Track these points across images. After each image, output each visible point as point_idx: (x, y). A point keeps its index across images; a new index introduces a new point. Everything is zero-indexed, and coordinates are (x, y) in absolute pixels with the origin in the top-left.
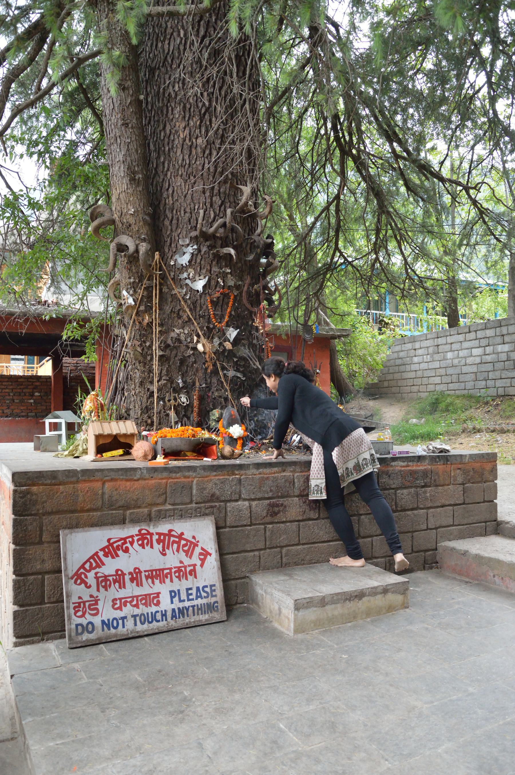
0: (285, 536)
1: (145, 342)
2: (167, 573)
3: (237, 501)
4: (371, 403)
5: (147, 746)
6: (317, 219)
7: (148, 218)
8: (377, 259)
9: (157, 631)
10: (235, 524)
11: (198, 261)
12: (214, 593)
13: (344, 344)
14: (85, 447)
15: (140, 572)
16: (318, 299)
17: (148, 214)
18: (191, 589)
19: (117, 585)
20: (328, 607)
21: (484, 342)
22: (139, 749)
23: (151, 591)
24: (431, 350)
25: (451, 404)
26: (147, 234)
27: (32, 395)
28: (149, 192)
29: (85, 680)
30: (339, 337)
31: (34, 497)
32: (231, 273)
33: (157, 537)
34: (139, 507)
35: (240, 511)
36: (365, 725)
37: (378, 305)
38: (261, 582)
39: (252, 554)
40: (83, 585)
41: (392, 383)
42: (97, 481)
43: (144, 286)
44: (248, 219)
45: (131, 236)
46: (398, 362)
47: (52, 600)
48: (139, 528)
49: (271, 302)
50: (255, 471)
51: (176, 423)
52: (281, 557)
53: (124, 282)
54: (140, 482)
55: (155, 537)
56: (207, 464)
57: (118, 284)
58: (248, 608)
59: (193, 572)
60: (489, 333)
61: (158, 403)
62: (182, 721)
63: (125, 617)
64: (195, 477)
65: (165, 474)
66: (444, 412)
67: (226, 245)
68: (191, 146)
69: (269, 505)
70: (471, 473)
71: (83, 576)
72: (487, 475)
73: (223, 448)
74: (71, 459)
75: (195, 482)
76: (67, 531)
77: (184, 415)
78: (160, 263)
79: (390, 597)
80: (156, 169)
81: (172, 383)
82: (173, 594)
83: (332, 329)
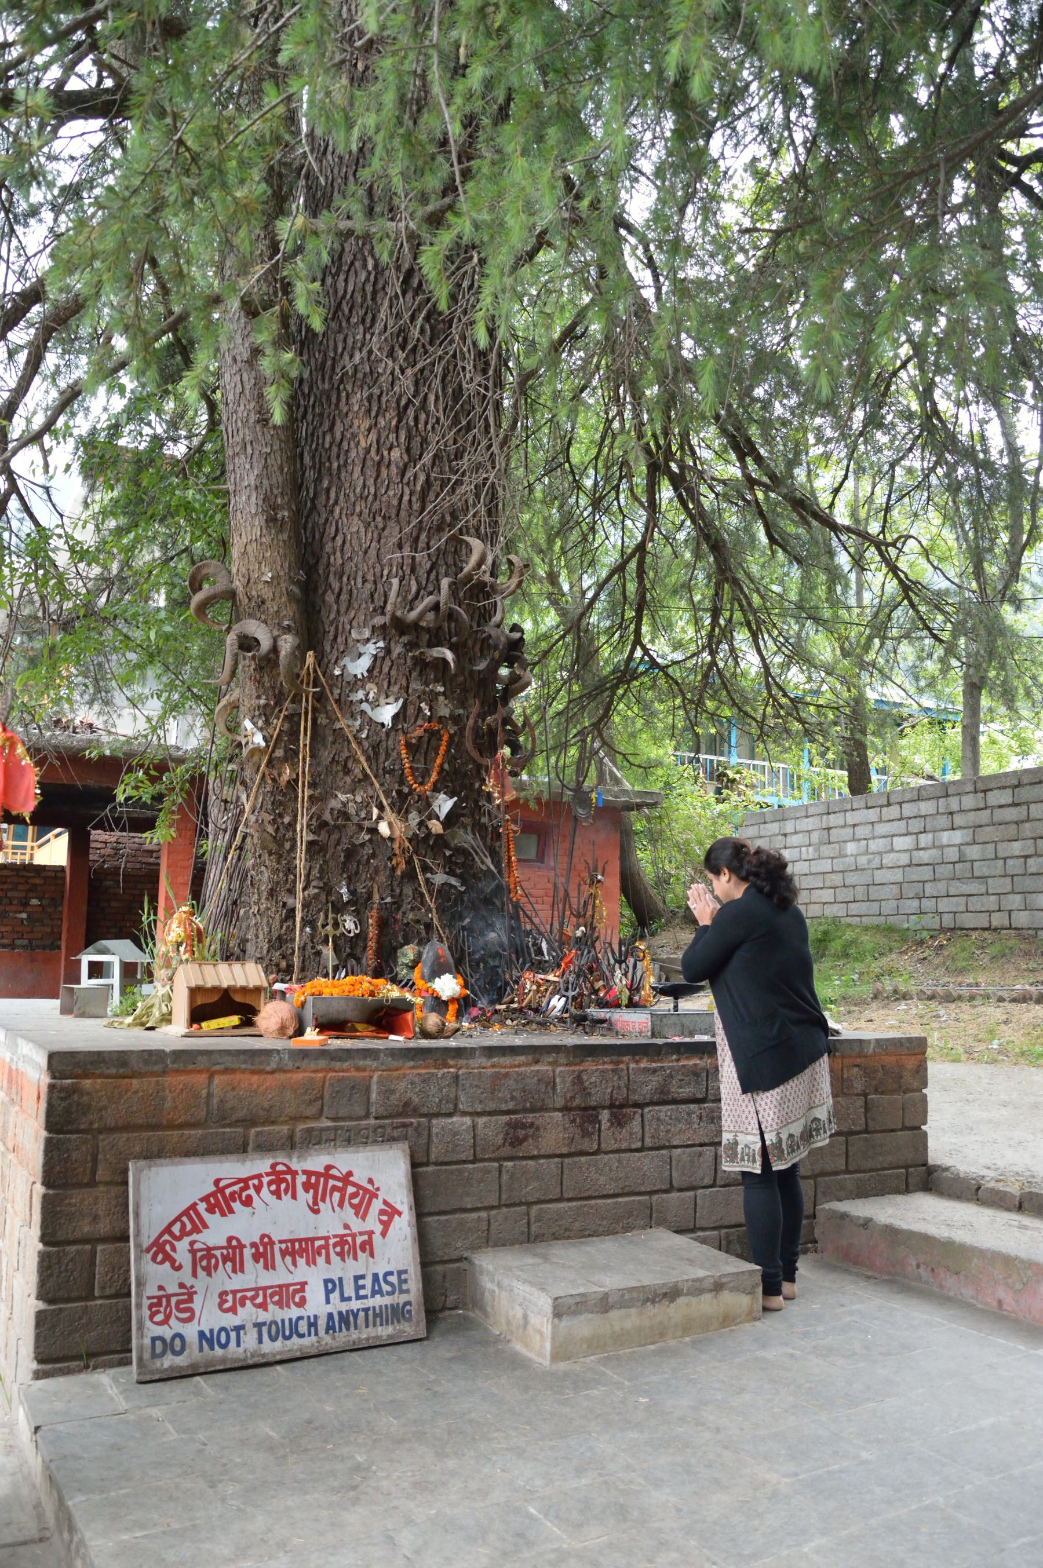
0: (536, 1184)
1: (281, 816)
2: (321, 1247)
3: (450, 1115)
5: (296, 1541)
6: (601, 586)
7: (296, 590)
8: (713, 663)
9: (298, 1354)
11: (386, 669)
13: (649, 820)
14: (164, 1010)
15: (272, 1243)
16: (600, 735)
17: (298, 583)
18: (363, 1277)
19: (229, 1264)
20: (614, 1314)
21: (916, 825)
22: (282, 1545)
23: (289, 1279)
24: (815, 837)
25: (854, 942)
26: (293, 619)
27: (25, 904)
28: (299, 541)
29: (173, 1436)
30: (639, 807)
31: (85, 1098)
32: (444, 694)
33: (304, 1178)
34: (273, 1123)
35: (455, 1134)
36: (679, 1511)
37: (717, 744)
38: (491, 1268)
39: (474, 1215)
40: (167, 1264)
42: (200, 1072)
43: (284, 713)
44: (478, 594)
45: (265, 622)
47: (108, 1292)
48: (271, 1161)
49: (515, 748)
50: (483, 1061)
51: (336, 969)
53: (247, 704)
54: (277, 1076)
55: (301, 1179)
56: (398, 1045)
57: (235, 706)
58: (465, 1318)
59: (368, 1246)
60: (926, 807)
61: (302, 930)
62: (356, 1501)
64: (377, 1069)
65: (322, 1063)
66: (839, 958)
67: (436, 641)
68: (379, 464)
70: (880, 1075)
71: (168, 1248)
72: (908, 1079)
73: (425, 1019)
74: (139, 1032)
75: (375, 1079)
76: (142, 1163)
77: (350, 952)
80: (313, 500)
81: (329, 893)
82: (330, 1286)
83: (625, 792)
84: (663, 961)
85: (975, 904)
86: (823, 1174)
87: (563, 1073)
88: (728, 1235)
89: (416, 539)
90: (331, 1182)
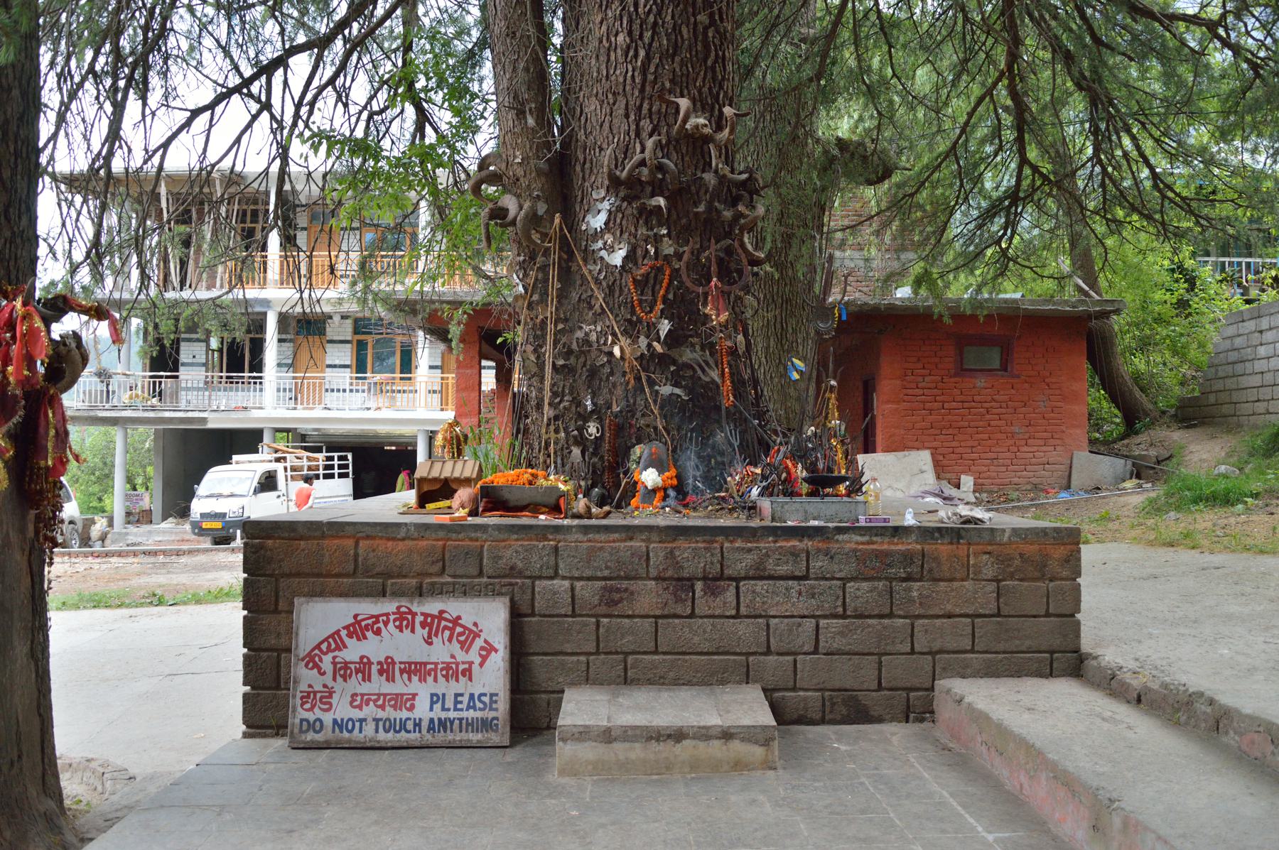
2: (430, 670)
3: (552, 578)
10: (547, 613)
12: (494, 706)
15: (394, 663)
18: (462, 695)
19: (360, 675)
20: (616, 745)
23: (404, 690)
26: (542, 190)
33: (422, 618)
34: (405, 577)
35: (555, 594)
39: (575, 658)
41: (1224, 397)
46: (1233, 356)
50: (581, 537)
52: (626, 670)
55: (419, 619)
59: (468, 673)
63: (365, 720)
69: (604, 588)
70: (1017, 562)
76: (303, 599)
78: (561, 229)
79: (737, 746)
82: (435, 699)
84: (1135, 458)
86: (940, 652)
87: (658, 551)
88: (831, 698)
89: (640, 108)
90: (443, 623)
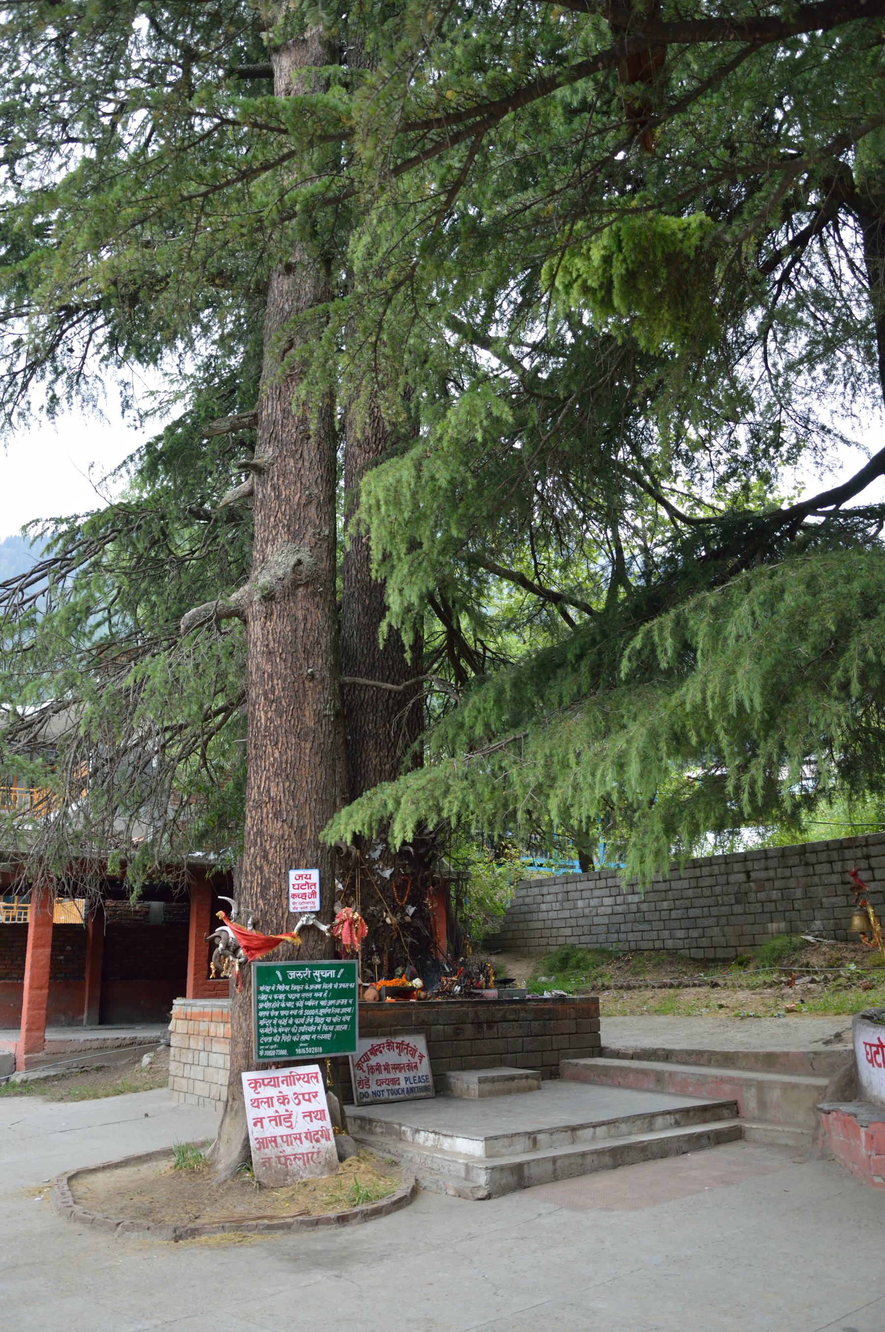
4: (493, 959)
24: (560, 897)
46: (524, 909)
82: (407, 1079)
85: (647, 936)
